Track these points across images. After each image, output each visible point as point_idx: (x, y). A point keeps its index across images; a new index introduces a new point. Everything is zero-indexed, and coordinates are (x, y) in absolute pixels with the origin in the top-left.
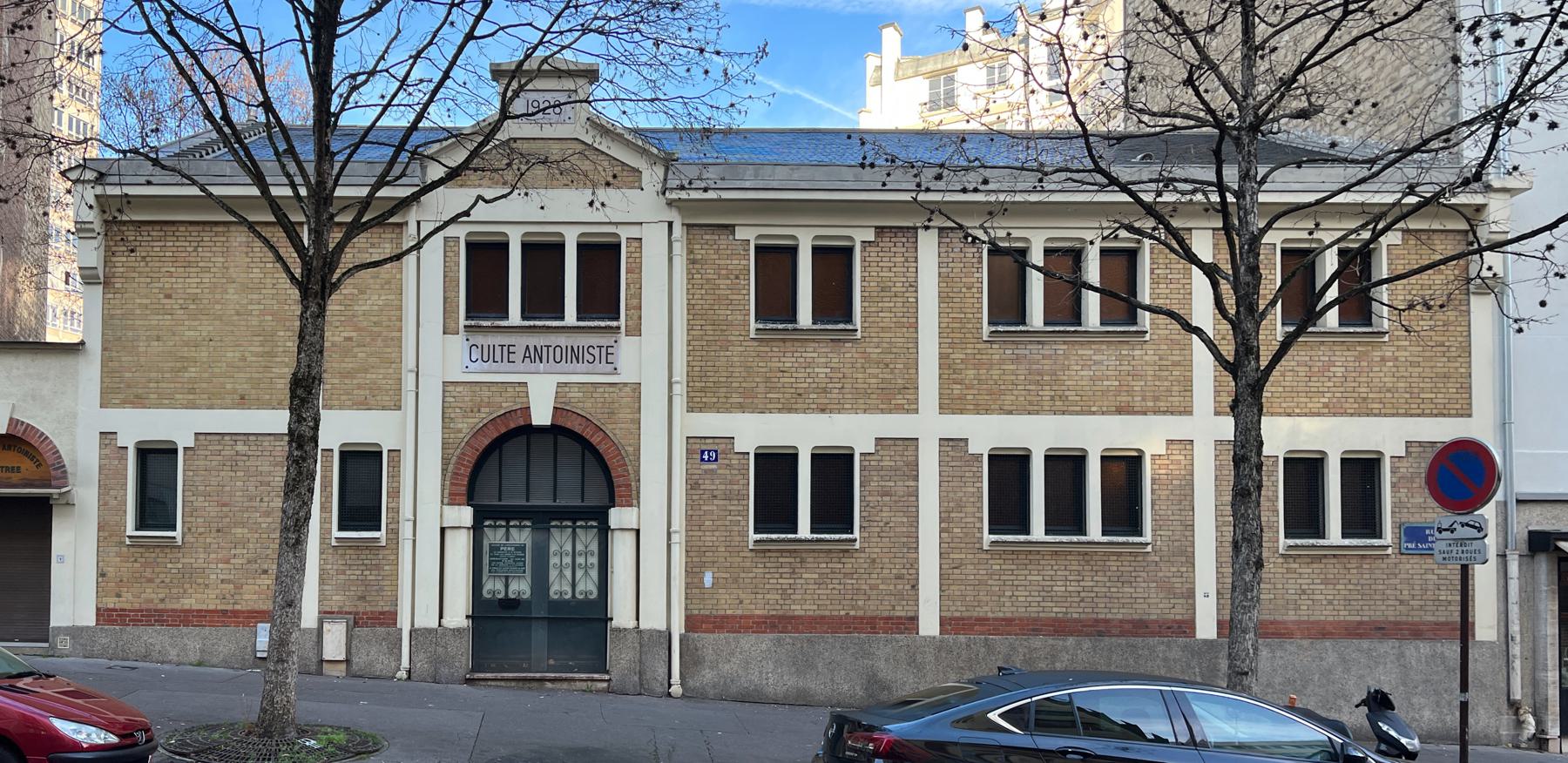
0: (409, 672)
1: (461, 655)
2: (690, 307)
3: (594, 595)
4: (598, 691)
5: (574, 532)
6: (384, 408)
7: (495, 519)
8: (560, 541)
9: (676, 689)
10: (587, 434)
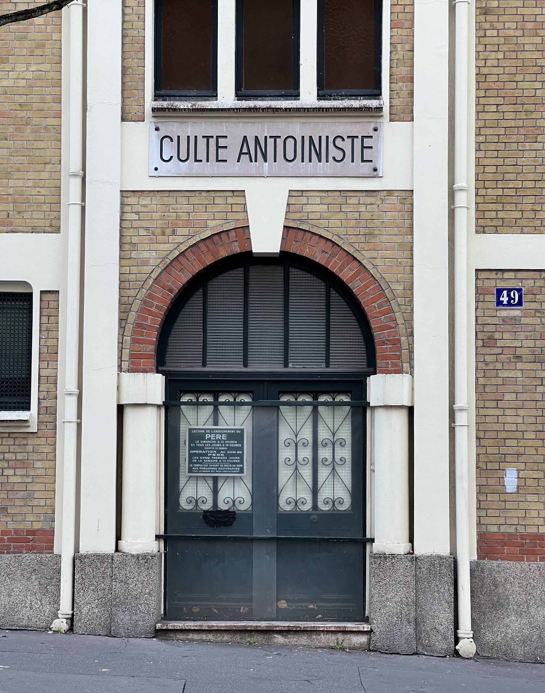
0: (71, 620)
1: (149, 594)
2: (481, 78)
3: (346, 506)
4: (353, 649)
5: (216, 411)
6: (34, 230)
7: (198, 392)
8: (293, 423)
9: (467, 646)
10: (334, 266)
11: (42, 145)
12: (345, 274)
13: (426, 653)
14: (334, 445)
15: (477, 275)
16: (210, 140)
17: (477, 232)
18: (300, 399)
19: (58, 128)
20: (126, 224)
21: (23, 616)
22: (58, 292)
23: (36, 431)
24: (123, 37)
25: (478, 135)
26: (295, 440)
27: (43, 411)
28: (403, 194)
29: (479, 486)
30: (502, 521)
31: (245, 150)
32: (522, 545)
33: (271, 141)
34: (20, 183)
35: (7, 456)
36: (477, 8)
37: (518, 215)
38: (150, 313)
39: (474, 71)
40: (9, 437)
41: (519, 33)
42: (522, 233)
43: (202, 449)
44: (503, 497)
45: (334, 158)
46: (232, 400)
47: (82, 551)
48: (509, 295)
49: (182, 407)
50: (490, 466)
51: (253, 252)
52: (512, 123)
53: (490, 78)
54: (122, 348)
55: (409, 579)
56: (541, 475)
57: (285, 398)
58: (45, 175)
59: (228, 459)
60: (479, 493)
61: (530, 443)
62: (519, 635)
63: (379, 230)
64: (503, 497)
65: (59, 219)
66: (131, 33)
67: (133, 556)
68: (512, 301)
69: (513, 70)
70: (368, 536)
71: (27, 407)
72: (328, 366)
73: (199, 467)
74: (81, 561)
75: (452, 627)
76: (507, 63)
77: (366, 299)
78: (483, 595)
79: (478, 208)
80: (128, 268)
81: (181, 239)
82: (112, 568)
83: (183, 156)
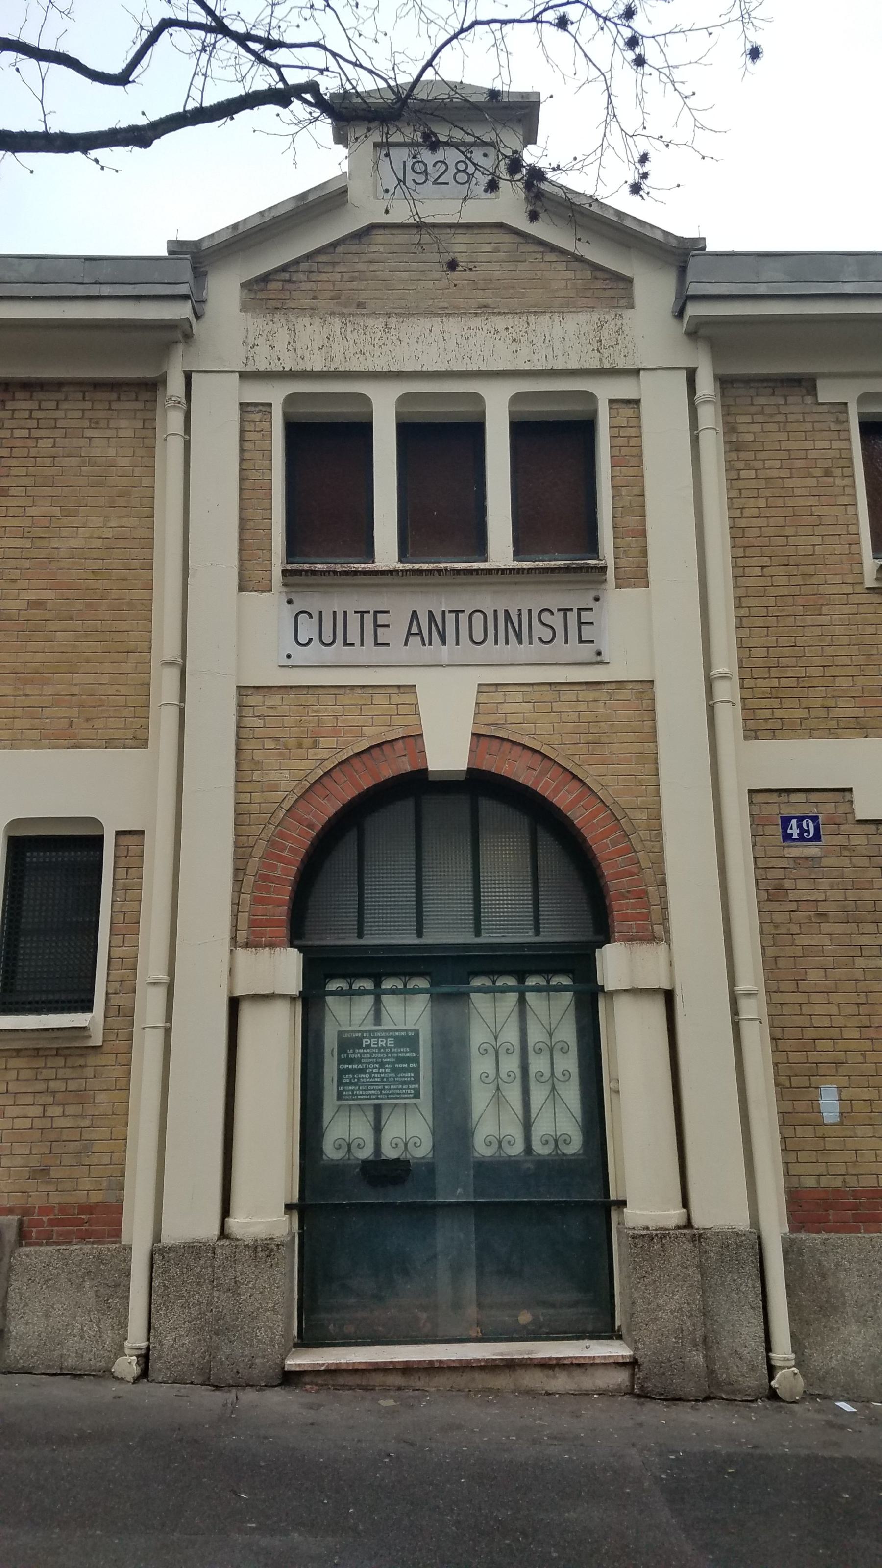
0: (145, 1358)
2: (737, 532)
3: (574, 1146)
5: (378, 1002)
6: (109, 744)
8: (490, 1014)
9: (787, 1379)
11: (123, 626)
12: (562, 798)
13: (724, 1396)
14: (551, 1050)
15: (750, 798)
16: (365, 615)
17: (746, 738)
18: (499, 983)
19: (147, 606)
20: (245, 733)
21: (68, 1350)
22: (142, 832)
23: (100, 1044)
24: (242, 479)
25: (738, 607)
26: (494, 1043)
27: (113, 1011)
28: (639, 686)
29: (782, 1114)
30: (821, 1168)
31: (415, 629)
32: (856, 1207)
33: (450, 618)
34: (90, 679)
35: (53, 1085)
36: (725, 443)
37: (803, 713)
38: (281, 859)
39: (727, 523)
40: (56, 1055)
41: (784, 473)
42: (811, 737)
43: (359, 1061)
44: (820, 1131)
45: (540, 638)
46: (401, 986)
47: (168, 1238)
48: (800, 826)
49: (329, 999)
50: (795, 1081)
51: (430, 769)
52: (785, 591)
53: (750, 533)
54: (238, 911)
55: (690, 1272)
56: (872, 1094)
57: (477, 982)
58: (127, 668)
59: (397, 1077)
60: (783, 1124)
61: (853, 1045)
62: (864, 1355)
63: (608, 736)
64: (820, 1131)
65: (148, 728)
66: (253, 475)
67: (247, 1246)
68: (806, 834)
69: (781, 521)
70: (613, 1196)
71: (86, 1006)
72: (537, 932)
73: (353, 1091)
74: (164, 1257)
75: (762, 1350)
76: (772, 512)
77: (593, 834)
78: (804, 1292)
79: (745, 704)
80: (249, 795)
81: (325, 754)
82: (213, 1267)
83: (327, 639)
